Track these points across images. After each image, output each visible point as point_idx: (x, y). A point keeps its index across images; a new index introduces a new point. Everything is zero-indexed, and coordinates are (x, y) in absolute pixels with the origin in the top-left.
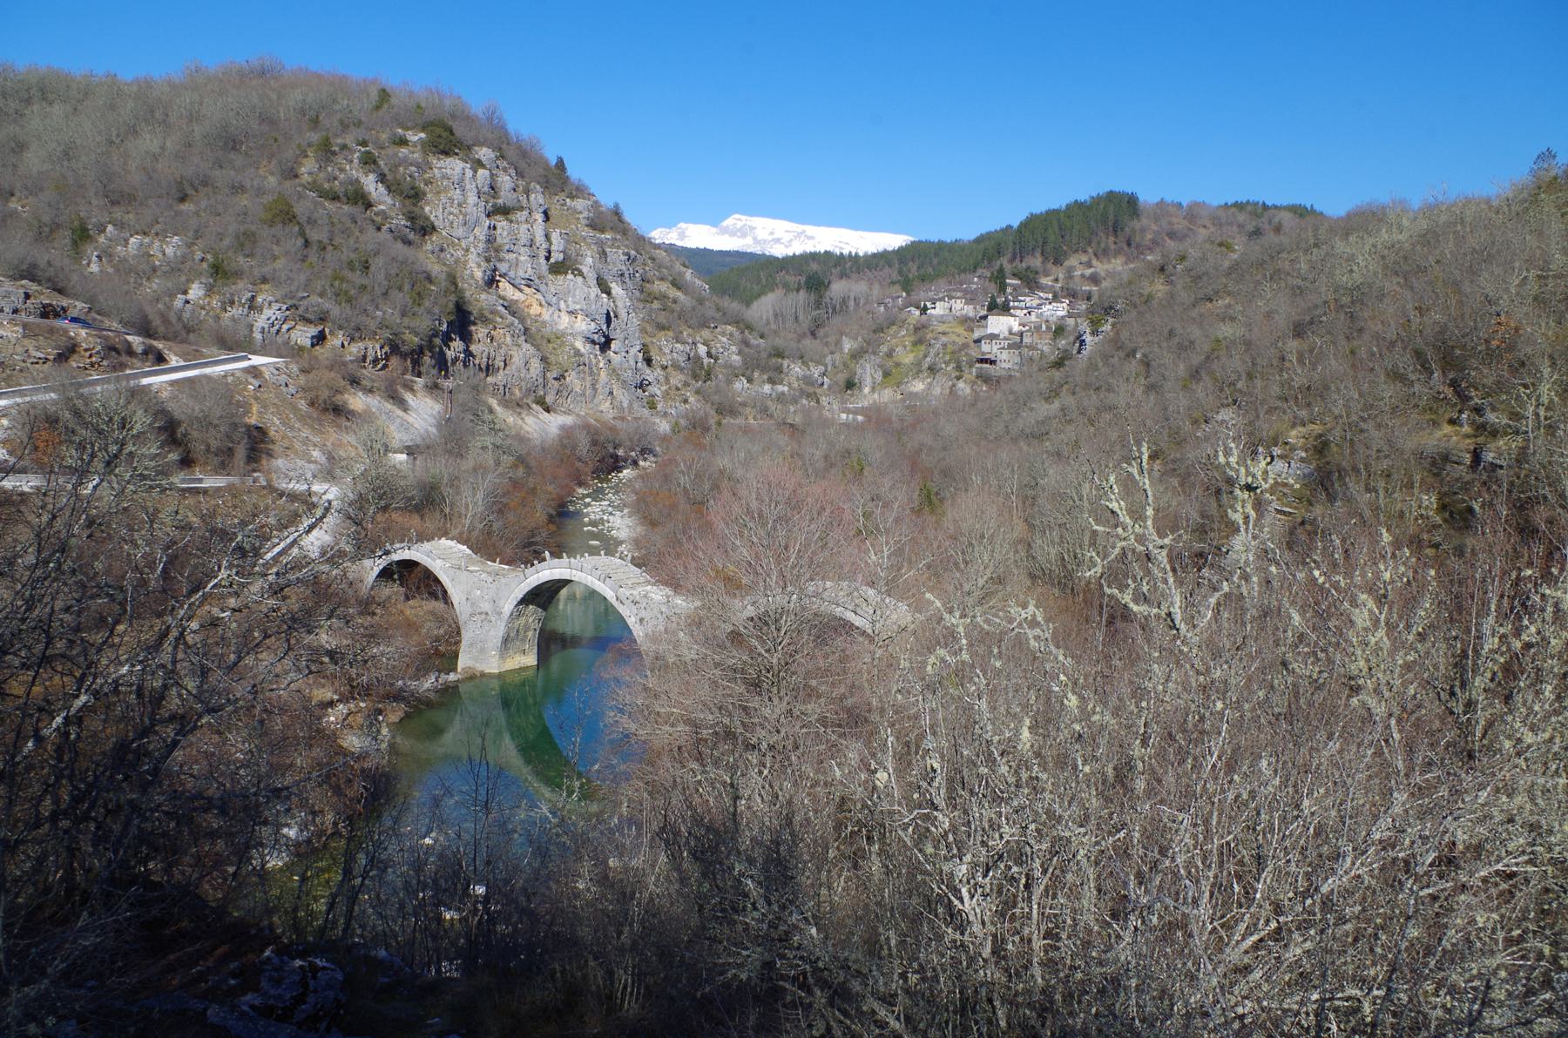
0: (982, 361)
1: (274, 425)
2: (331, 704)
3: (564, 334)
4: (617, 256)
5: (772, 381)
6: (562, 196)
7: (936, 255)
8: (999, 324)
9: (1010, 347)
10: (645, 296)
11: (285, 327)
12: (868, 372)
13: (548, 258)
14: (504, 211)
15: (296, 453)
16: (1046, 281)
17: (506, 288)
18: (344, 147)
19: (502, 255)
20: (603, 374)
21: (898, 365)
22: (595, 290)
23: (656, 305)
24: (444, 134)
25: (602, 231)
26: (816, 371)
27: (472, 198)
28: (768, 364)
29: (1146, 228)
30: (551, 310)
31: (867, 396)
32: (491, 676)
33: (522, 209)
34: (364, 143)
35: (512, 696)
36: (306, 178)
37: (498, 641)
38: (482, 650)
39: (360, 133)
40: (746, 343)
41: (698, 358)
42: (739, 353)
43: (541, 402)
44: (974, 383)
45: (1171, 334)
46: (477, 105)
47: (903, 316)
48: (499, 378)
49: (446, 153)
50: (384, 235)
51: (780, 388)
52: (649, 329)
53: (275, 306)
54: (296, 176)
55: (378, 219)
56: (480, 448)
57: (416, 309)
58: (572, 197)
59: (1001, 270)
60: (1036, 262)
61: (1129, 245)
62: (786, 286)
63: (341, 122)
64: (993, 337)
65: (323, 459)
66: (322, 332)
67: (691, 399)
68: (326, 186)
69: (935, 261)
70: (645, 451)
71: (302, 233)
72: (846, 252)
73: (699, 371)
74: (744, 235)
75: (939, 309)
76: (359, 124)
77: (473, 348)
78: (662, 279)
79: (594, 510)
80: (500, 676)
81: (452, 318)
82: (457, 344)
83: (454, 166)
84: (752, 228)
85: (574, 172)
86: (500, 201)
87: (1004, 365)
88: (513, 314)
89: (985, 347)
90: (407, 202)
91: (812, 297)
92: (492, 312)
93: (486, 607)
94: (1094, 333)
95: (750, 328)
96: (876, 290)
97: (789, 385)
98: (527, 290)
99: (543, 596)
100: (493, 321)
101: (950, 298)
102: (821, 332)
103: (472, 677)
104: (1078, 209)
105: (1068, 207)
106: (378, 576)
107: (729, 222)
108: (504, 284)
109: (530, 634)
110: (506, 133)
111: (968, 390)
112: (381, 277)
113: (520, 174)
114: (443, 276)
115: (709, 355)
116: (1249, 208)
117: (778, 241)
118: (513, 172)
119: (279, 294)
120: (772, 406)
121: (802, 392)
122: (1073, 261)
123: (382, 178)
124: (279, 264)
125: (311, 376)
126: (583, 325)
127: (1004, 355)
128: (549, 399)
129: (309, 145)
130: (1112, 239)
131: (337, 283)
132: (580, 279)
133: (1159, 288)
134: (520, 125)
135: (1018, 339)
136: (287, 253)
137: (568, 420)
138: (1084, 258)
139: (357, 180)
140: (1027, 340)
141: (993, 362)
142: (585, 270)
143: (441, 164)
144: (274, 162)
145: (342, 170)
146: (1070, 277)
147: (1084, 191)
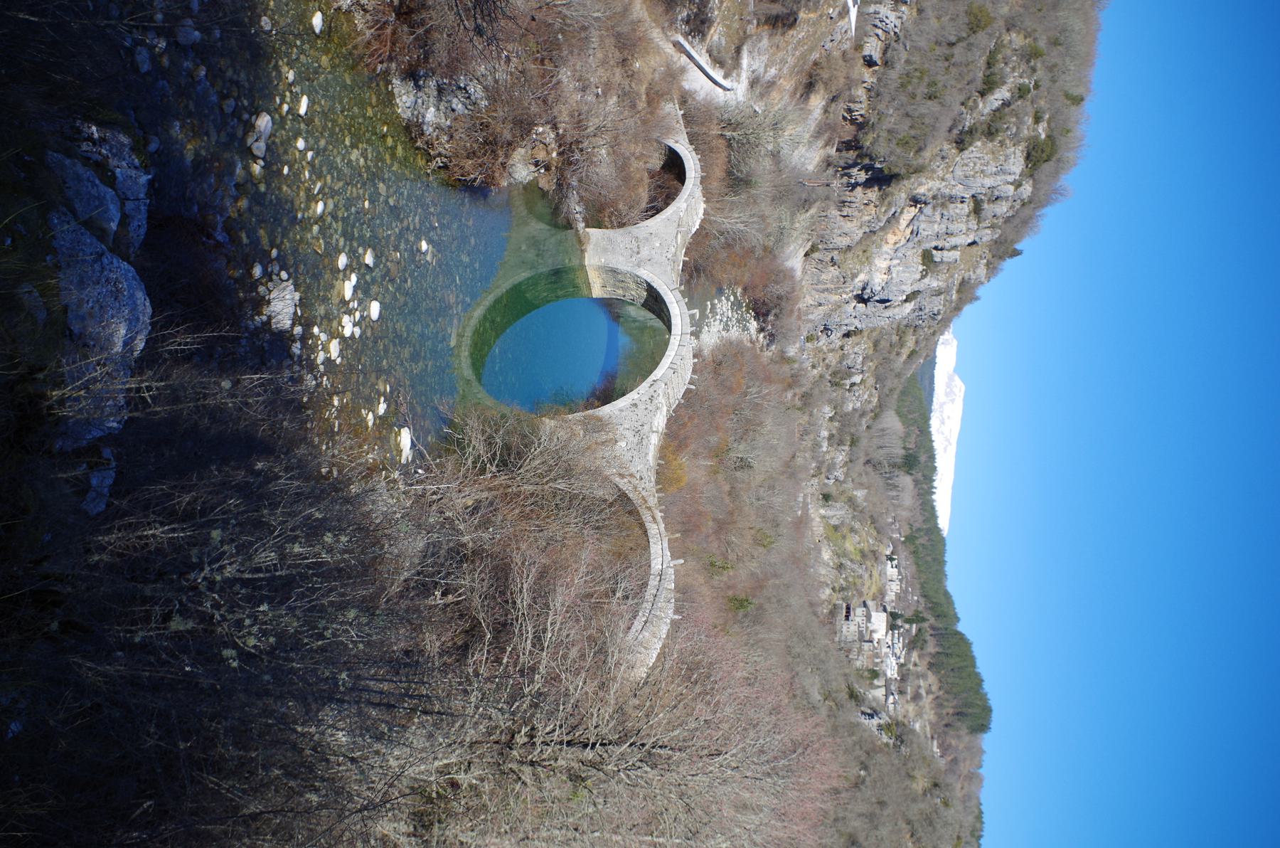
0: (848, 608)
1: (798, 33)
2: (555, 127)
3: (870, 263)
4: (937, 304)
5: (831, 437)
6: (989, 256)
7: (934, 560)
8: (879, 621)
9: (860, 632)
10: (902, 330)
11: (880, 32)
12: (837, 513)
13: (936, 248)
14: (977, 210)
15: (774, 54)
16: (915, 656)
17: (911, 212)
18: (1034, 70)
19: (939, 209)
20: (837, 298)
21: (844, 537)
22: (909, 290)
23: (895, 338)
24: (1044, 156)
25: (958, 291)
26: (839, 473)
27: (989, 182)
28: (845, 434)
29: (959, 740)
30: (891, 252)
31: (817, 513)
32: (582, 258)
33: (979, 222)
34: (1037, 86)
35: (563, 279)
36: (1006, 38)
37: (613, 265)
38: (605, 250)
39: (1045, 83)
40: (863, 414)
41: (850, 375)
42: (854, 410)
43: (814, 249)
44: (829, 602)
45: (882, 804)
46: (1068, 180)
47: (885, 541)
48: (834, 212)
49: (1028, 157)
50: (958, 108)
51: (825, 444)
52: (874, 334)
53: (898, 23)
54: (1008, 30)
55: (970, 103)
56: (777, 214)
57: (894, 142)
58: (988, 264)
59: (924, 620)
60: (931, 648)
61: (946, 725)
62: (907, 435)
63: (1055, 65)
64: (868, 617)
65: (768, 77)
66: (875, 64)
67: (815, 371)
68: (1000, 56)
69: (929, 559)
70: (772, 338)
71: (960, 40)
72: (935, 484)
73: (839, 377)
74: (947, 394)
75: (891, 572)
76: (1054, 81)
77: (859, 189)
78: (917, 342)
79: (724, 306)
80: (583, 267)
81: (886, 172)
82: (862, 177)
83: (1017, 164)
84: (953, 401)
85: (1009, 264)
86: (986, 206)
87: (844, 629)
88: (888, 221)
89: (860, 611)
90: (985, 127)
91: (899, 461)
92: (890, 204)
93: (645, 252)
94: (880, 727)
95: (876, 417)
96: (905, 514)
97: (828, 452)
98: (909, 231)
99: (655, 302)
100: (882, 204)
101: (901, 580)
102: (869, 469)
103: (580, 242)
104: (977, 682)
105: (978, 674)
106: (670, 149)
107: (958, 382)
108: (913, 211)
109: (620, 292)
110: (1043, 206)
111: (823, 597)
112: (923, 110)
113: (1008, 220)
114: (920, 161)
115: (853, 385)
116: (978, 825)
117: (943, 423)
118: (1010, 214)
119: (909, 25)
120: (808, 443)
121: (821, 463)
122: (932, 678)
123: (1006, 104)
124: (933, 22)
125: (841, 62)
126: (878, 280)
127: (853, 628)
128: (816, 255)
129: (1035, 39)
130: (951, 711)
131: (918, 74)
132: (918, 276)
133: (920, 784)
134: (1050, 217)
135: (867, 638)
136: (943, 28)
137: (799, 273)
138: (934, 688)
139: (1004, 83)
140: (866, 646)
141: (847, 618)
142: (926, 280)
143: (1019, 154)
144: (1021, 10)
145: (1013, 69)
146: (918, 676)
147: (994, 689)
